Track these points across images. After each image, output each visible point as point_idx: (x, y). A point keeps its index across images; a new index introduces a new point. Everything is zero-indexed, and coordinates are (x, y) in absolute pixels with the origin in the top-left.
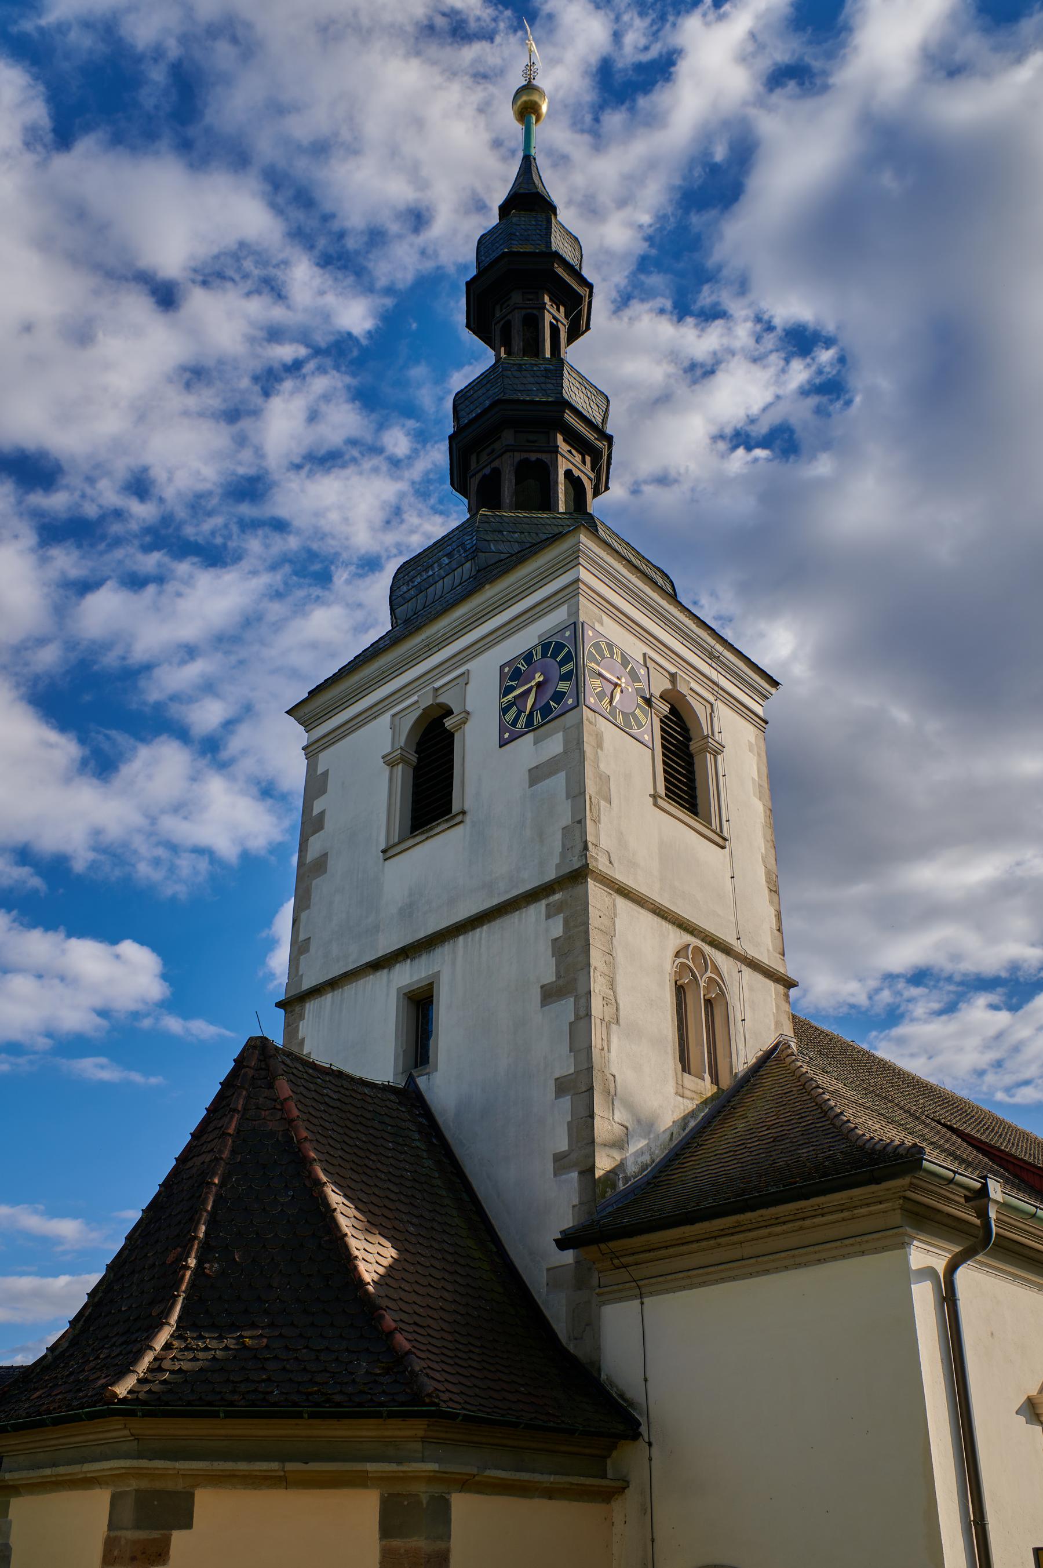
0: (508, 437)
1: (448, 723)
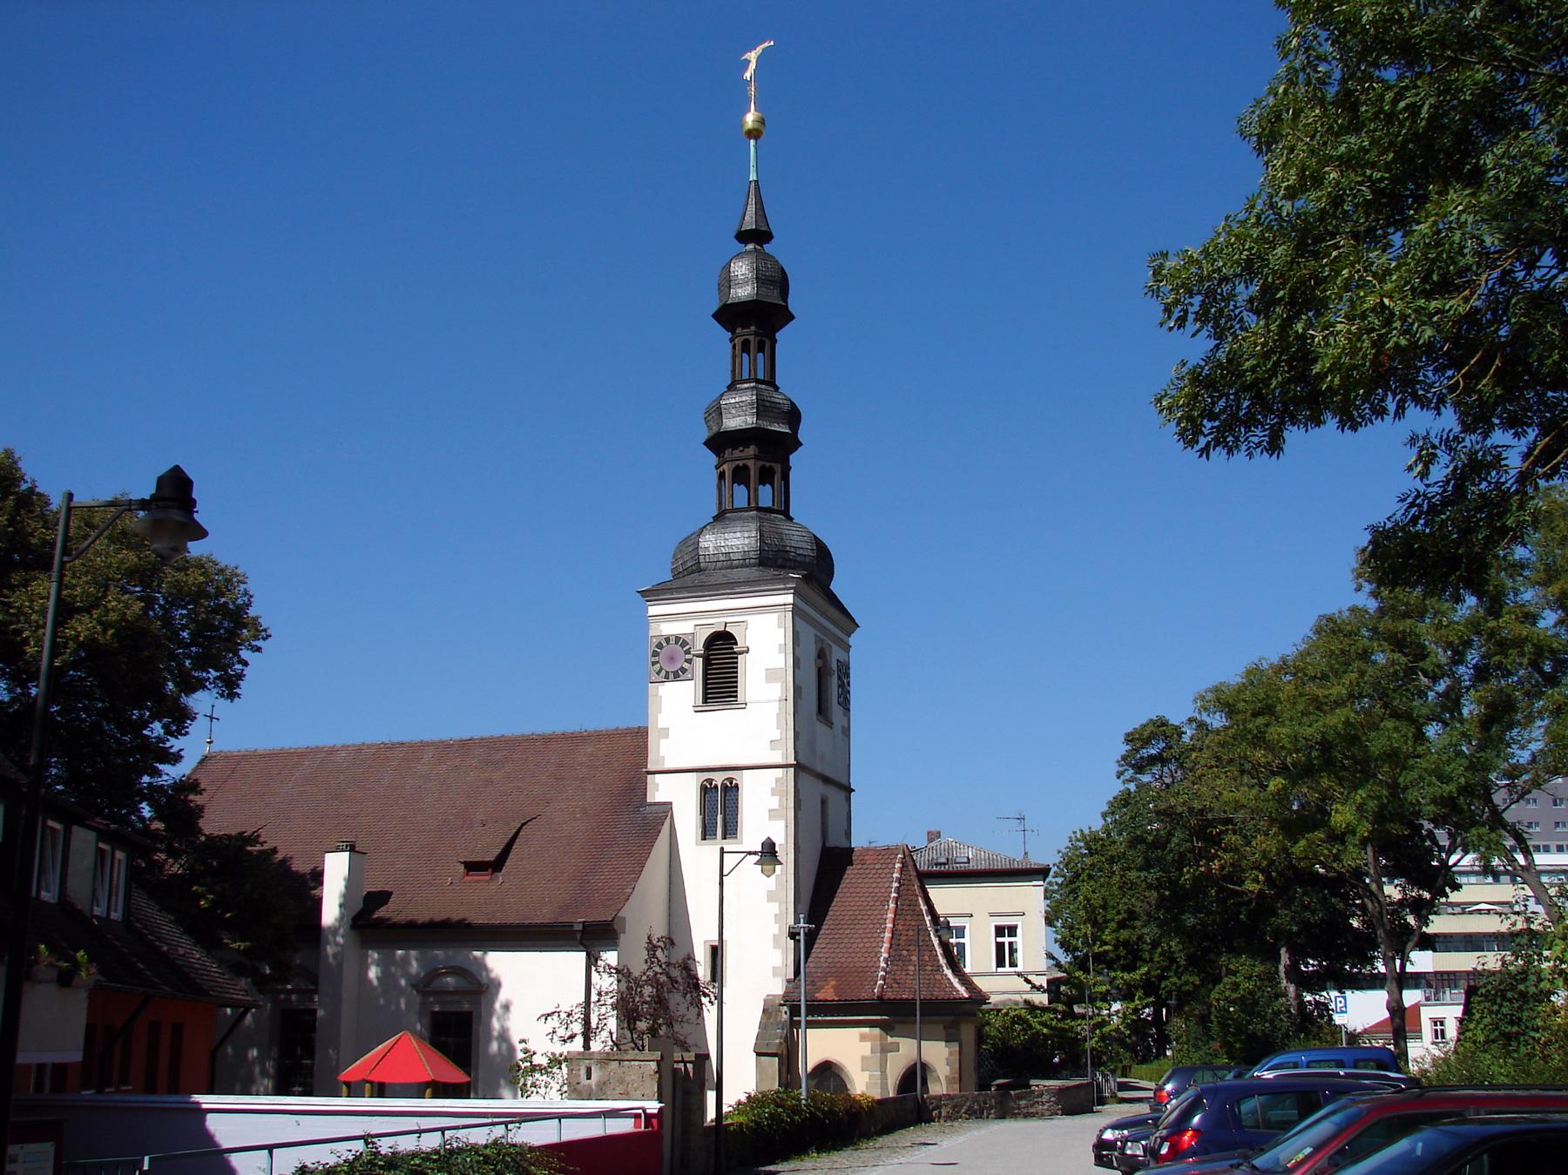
0: (752, 450)
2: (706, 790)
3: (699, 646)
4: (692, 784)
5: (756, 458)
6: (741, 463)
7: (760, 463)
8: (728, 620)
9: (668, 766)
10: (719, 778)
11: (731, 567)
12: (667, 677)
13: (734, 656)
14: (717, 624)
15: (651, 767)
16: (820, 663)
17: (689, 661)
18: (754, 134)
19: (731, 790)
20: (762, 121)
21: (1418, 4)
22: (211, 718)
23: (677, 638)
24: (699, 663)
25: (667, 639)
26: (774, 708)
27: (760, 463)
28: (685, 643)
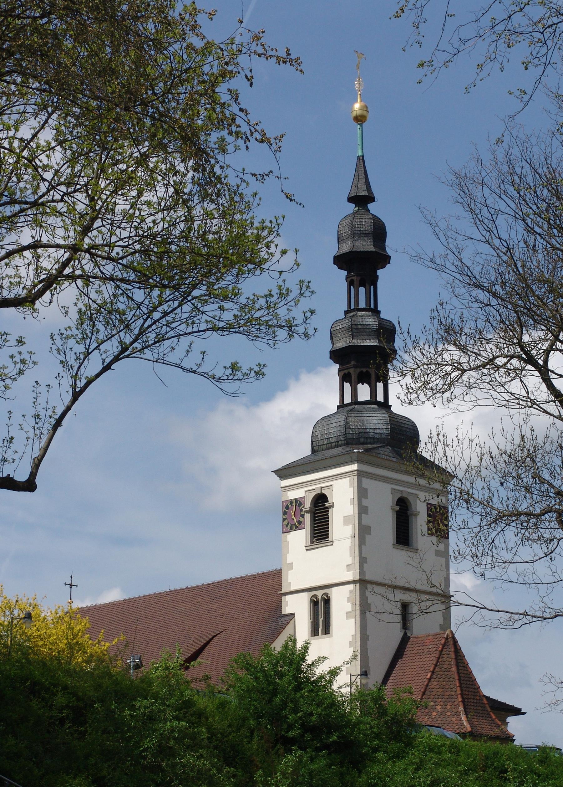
1: (327, 505)
2: (314, 603)
3: (308, 505)
4: (305, 598)
5: (355, 367)
6: (346, 371)
7: (358, 370)
8: (322, 485)
9: (293, 588)
10: (319, 593)
11: (331, 448)
12: (291, 528)
13: (326, 510)
14: (316, 488)
15: (284, 590)
16: (398, 508)
17: (303, 516)
18: (360, 120)
19: (327, 601)
20: (365, 108)
21: (170, 1)
22: (71, 585)
23: (297, 500)
24: (308, 517)
25: (291, 502)
26: (348, 543)
27: (358, 370)
28: (300, 504)
